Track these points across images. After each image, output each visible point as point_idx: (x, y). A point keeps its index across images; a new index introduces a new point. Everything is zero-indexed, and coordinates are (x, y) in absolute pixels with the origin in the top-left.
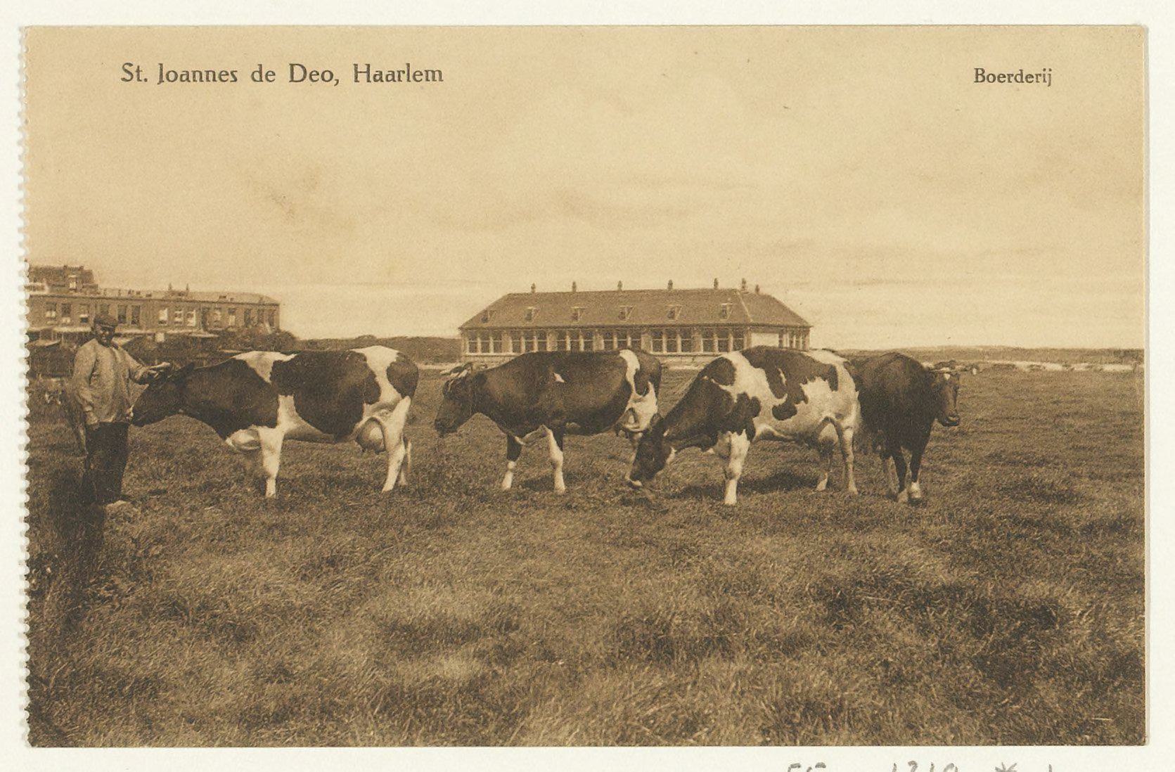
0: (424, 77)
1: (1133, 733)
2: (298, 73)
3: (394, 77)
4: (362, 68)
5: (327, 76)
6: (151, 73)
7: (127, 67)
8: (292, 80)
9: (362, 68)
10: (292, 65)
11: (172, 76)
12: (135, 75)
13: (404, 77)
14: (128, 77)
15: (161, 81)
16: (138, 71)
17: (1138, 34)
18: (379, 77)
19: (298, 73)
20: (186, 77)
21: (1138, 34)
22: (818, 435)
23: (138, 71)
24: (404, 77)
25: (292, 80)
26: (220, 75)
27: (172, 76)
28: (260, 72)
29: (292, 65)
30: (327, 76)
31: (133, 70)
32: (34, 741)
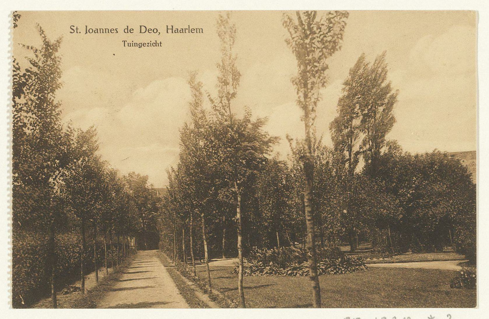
0: (195, 31)
2: (143, 29)
3: (182, 31)
4: (170, 27)
5: (155, 31)
6: (82, 30)
7: (72, 27)
8: (141, 32)
9: (170, 27)
10: (141, 26)
12: (76, 31)
13: (187, 31)
14: (73, 31)
15: (86, 33)
16: (77, 29)
18: (177, 31)
19: (143, 29)
20: (96, 31)
24: (187, 31)
25: (141, 32)
27: (91, 31)
29: (141, 26)
30: (155, 31)
31: (75, 28)
32: (17, 304)
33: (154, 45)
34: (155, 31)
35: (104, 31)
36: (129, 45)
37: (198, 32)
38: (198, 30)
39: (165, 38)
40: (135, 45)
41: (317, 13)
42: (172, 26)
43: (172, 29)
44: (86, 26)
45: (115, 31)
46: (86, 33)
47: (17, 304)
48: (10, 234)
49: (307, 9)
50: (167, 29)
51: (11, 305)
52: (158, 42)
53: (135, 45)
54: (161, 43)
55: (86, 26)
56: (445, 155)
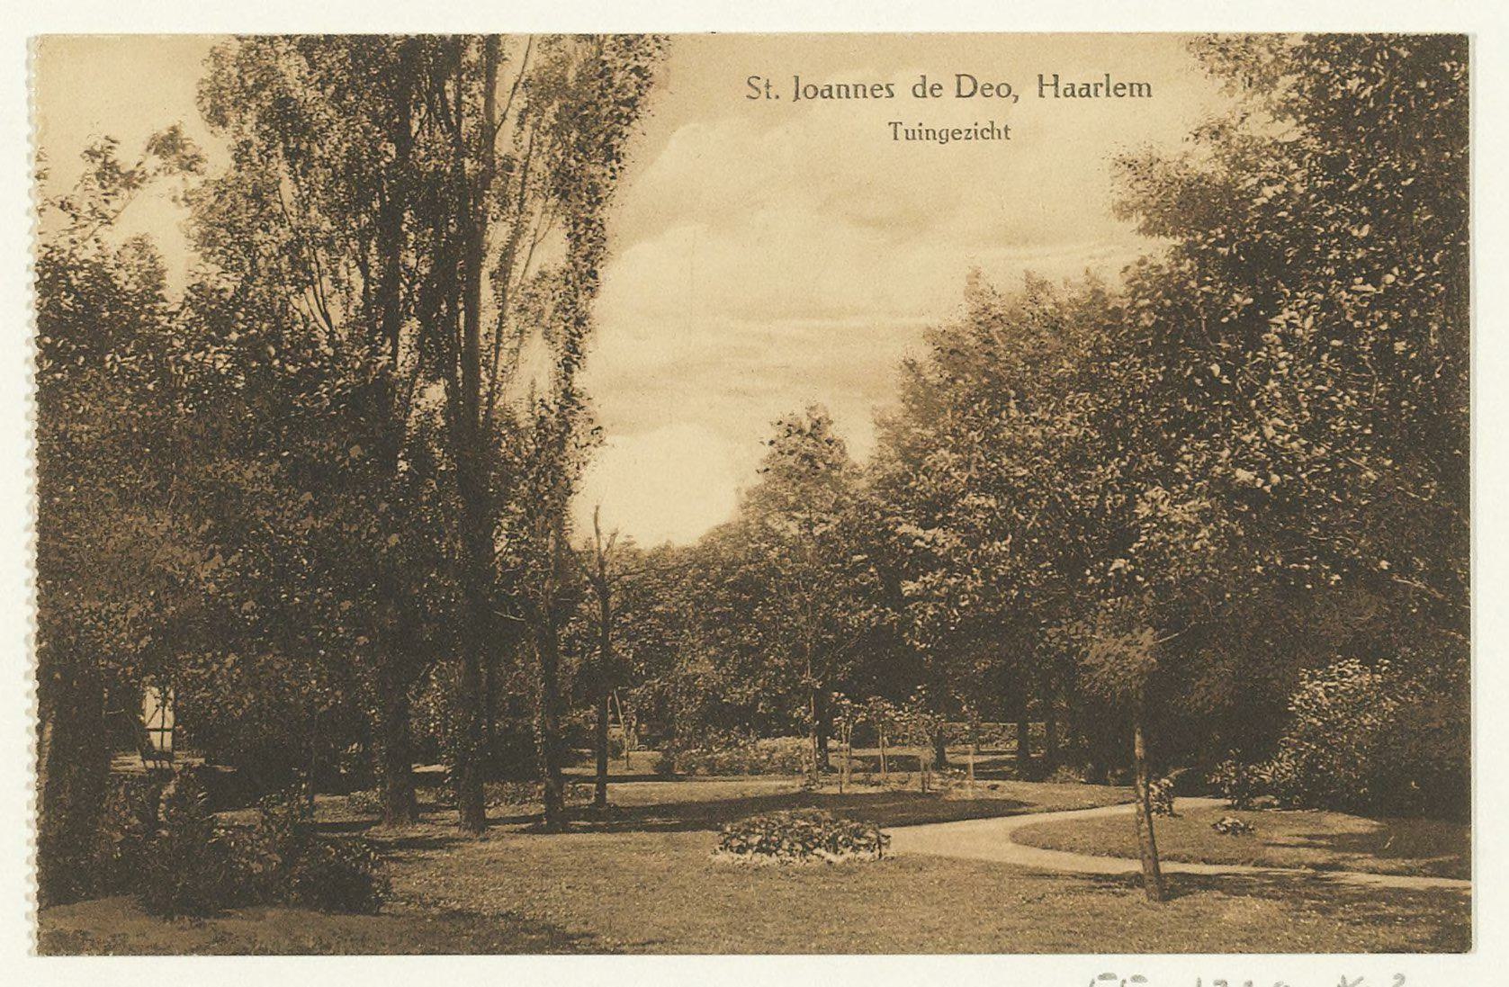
0: (1127, 91)
1: (1453, 935)
3: (1087, 91)
4: (1048, 79)
5: (1004, 90)
7: (753, 81)
9: (1048, 79)
11: (811, 92)
12: (763, 90)
13: (1102, 91)
14: (755, 94)
15: (797, 97)
16: (768, 86)
17: (1454, 47)
18: (1072, 92)
19: (967, 87)
21: (1454, 47)
22: (510, 469)
23: (768, 86)
24: (1102, 91)
26: (932, 89)
28: (924, 86)
30: (1004, 90)
31: (761, 84)
32: (54, 943)
33: (986, 134)
34: (1007, 91)
35: (852, 93)
36: (911, 136)
37: (1136, 93)
38: (1136, 88)
39: (1029, 109)
40: (930, 134)
41: (507, 48)
42: (1056, 76)
43: (1056, 85)
44: (797, 78)
45: (885, 93)
46: (797, 97)
47: (54, 943)
48: (32, 703)
49: (656, 31)
50: (1041, 85)
51: (32, 943)
52: (999, 126)
53: (930, 134)
54: (1006, 129)
55: (797, 78)
56: (708, 546)
